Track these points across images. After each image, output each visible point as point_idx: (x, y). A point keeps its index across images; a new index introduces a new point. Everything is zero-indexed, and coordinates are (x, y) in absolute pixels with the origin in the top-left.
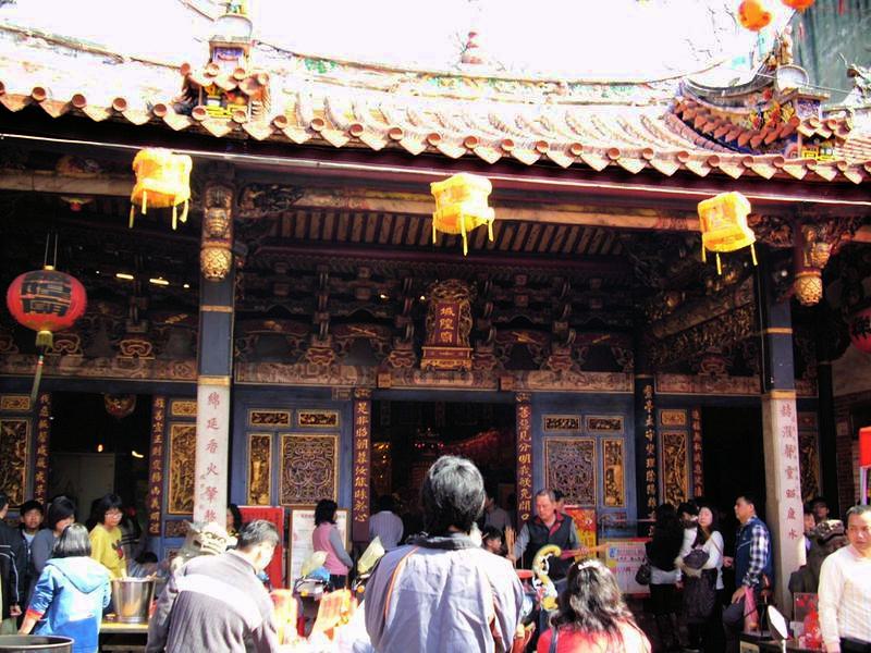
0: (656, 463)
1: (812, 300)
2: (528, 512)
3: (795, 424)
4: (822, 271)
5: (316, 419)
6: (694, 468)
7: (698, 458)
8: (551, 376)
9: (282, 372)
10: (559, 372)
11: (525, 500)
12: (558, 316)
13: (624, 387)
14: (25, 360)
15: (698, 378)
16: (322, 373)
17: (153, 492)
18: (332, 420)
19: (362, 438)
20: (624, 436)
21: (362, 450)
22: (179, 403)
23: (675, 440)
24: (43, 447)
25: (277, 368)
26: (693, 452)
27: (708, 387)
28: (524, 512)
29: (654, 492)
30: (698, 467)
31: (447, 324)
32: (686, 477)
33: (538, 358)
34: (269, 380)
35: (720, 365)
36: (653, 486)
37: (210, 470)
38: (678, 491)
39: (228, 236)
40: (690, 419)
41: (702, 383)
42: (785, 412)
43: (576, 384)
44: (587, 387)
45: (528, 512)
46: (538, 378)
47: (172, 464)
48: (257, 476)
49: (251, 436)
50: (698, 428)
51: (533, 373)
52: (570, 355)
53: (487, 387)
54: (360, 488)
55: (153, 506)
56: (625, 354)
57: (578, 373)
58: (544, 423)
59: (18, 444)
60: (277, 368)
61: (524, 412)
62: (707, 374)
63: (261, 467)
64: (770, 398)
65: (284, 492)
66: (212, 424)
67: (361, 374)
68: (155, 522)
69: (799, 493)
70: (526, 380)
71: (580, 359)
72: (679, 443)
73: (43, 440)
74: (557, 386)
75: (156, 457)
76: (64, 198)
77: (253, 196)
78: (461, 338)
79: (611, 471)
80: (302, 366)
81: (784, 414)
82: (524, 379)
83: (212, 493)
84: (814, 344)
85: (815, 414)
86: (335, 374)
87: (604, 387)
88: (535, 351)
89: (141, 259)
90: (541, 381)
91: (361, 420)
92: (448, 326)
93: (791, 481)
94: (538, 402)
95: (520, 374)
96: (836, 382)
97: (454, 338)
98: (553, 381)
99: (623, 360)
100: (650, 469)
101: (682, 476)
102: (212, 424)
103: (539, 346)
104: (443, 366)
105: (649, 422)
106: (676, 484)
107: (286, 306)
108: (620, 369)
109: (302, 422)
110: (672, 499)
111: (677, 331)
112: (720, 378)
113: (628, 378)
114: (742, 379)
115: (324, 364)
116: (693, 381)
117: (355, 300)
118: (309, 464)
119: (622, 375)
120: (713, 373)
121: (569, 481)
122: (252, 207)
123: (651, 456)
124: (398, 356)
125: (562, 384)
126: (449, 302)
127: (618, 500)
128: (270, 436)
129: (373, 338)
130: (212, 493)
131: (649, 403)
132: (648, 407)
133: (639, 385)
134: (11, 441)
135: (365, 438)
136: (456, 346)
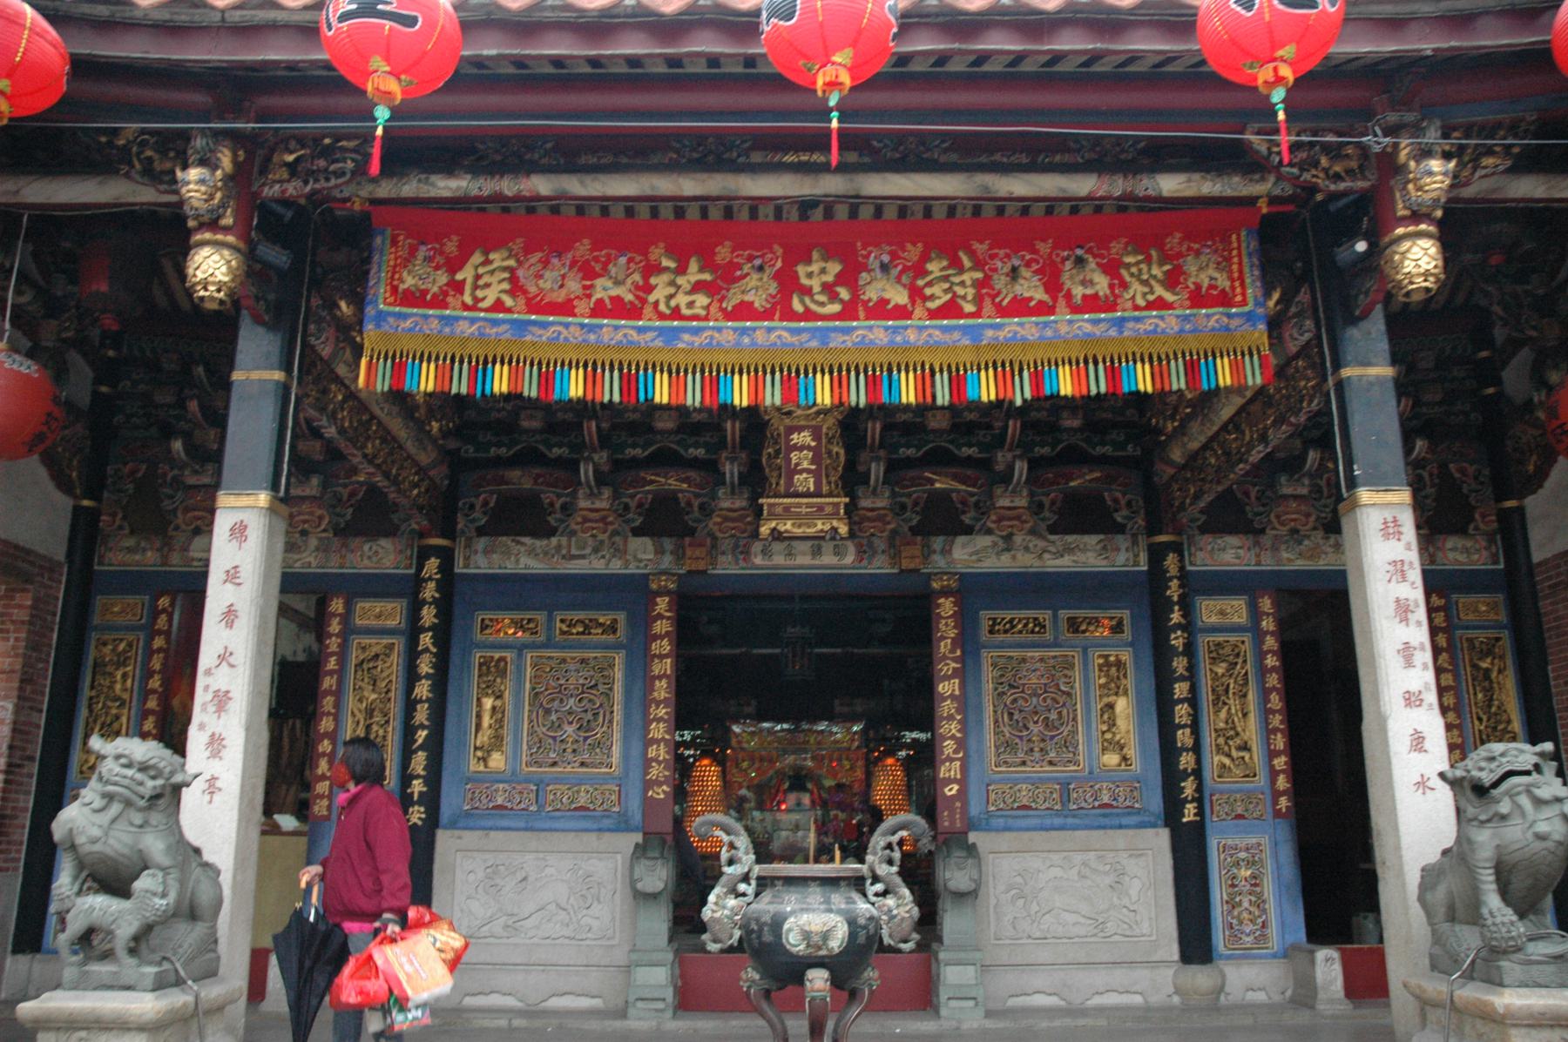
0: (1193, 689)
1: (1420, 282)
2: (955, 781)
4: (1440, 223)
5: (586, 627)
6: (1266, 700)
7: (1273, 680)
8: (995, 544)
9: (532, 552)
10: (1008, 538)
11: (952, 760)
12: (1000, 441)
13: (1122, 557)
14: (138, 544)
15: (1266, 540)
16: (596, 550)
17: (321, 749)
19: (662, 657)
20: (1131, 644)
21: (660, 678)
22: (367, 605)
23: (1227, 650)
24: (157, 677)
25: (523, 544)
26: (1263, 671)
27: (1285, 555)
28: (949, 781)
29: (1189, 742)
30: (1274, 697)
31: (802, 459)
32: (1252, 716)
33: (972, 514)
34: (510, 567)
35: (1308, 515)
36: (1188, 731)
37: (222, 658)
38: (1238, 741)
39: (228, 220)
40: (1255, 614)
41: (1275, 549)
42: (1390, 530)
43: (1040, 557)
44: (1058, 562)
45: (955, 781)
46: (970, 550)
47: (351, 702)
49: (477, 656)
50: (1272, 628)
51: (960, 540)
52: (1028, 508)
53: (880, 566)
54: (658, 742)
55: (320, 772)
56: (1129, 504)
57: (1045, 538)
58: (985, 625)
59: (119, 675)
60: (523, 544)
61: (947, 607)
62: (1283, 530)
63: (494, 708)
64: (1355, 505)
65: (530, 748)
66: (232, 576)
67: (660, 551)
68: (322, 797)
69: (1432, 697)
70: (950, 552)
71: (1047, 514)
72: (1238, 655)
73: (157, 667)
75: (328, 692)
77: (290, 158)
78: (829, 483)
79: (1111, 706)
80: (564, 540)
81: (1387, 536)
82: (946, 552)
84: (1487, 472)
85: (1500, 597)
86: (620, 552)
87: (1092, 561)
88: (964, 503)
90: (976, 553)
91: (661, 627)
92: (805, 465)
93: (1412, 672)
94: (977, 591)
95: (938, 542)
96: (1536, 535)
97: (818, 484)
98: (998, 554)
99: (1125, 512)
100: (1181, 701)
101: (1245, 715)
102: (232, 576)
103: (972, 495)
104: (798, 531)
105: (1176, 617)
106: (1234, 728)
107: (542, 448)
108: (1120, 529)
109: (563, 633)
110: (1229, 755)
111: (1203, 439)
112: (1308, 537)
113: (1135, 543)
115: (601, 537)
116: (1257, 543)
117: (651, 430)
118: (572, 701)
119: (1122, 541)
120: (1294, 531)
121: (1031, 726)
122: (286, 176)
123: (1182, 678)
124: (726, 519)
125: (1014, 557)
126: (802, 423)
127: (1125, 759)
129: (682, 491)
130: (221, 701)
131: (1174, 583)
132: (1174, 591)
133: (1156, 555)
134: (109, 669)
135: (666, 656)
136: (821, 496)
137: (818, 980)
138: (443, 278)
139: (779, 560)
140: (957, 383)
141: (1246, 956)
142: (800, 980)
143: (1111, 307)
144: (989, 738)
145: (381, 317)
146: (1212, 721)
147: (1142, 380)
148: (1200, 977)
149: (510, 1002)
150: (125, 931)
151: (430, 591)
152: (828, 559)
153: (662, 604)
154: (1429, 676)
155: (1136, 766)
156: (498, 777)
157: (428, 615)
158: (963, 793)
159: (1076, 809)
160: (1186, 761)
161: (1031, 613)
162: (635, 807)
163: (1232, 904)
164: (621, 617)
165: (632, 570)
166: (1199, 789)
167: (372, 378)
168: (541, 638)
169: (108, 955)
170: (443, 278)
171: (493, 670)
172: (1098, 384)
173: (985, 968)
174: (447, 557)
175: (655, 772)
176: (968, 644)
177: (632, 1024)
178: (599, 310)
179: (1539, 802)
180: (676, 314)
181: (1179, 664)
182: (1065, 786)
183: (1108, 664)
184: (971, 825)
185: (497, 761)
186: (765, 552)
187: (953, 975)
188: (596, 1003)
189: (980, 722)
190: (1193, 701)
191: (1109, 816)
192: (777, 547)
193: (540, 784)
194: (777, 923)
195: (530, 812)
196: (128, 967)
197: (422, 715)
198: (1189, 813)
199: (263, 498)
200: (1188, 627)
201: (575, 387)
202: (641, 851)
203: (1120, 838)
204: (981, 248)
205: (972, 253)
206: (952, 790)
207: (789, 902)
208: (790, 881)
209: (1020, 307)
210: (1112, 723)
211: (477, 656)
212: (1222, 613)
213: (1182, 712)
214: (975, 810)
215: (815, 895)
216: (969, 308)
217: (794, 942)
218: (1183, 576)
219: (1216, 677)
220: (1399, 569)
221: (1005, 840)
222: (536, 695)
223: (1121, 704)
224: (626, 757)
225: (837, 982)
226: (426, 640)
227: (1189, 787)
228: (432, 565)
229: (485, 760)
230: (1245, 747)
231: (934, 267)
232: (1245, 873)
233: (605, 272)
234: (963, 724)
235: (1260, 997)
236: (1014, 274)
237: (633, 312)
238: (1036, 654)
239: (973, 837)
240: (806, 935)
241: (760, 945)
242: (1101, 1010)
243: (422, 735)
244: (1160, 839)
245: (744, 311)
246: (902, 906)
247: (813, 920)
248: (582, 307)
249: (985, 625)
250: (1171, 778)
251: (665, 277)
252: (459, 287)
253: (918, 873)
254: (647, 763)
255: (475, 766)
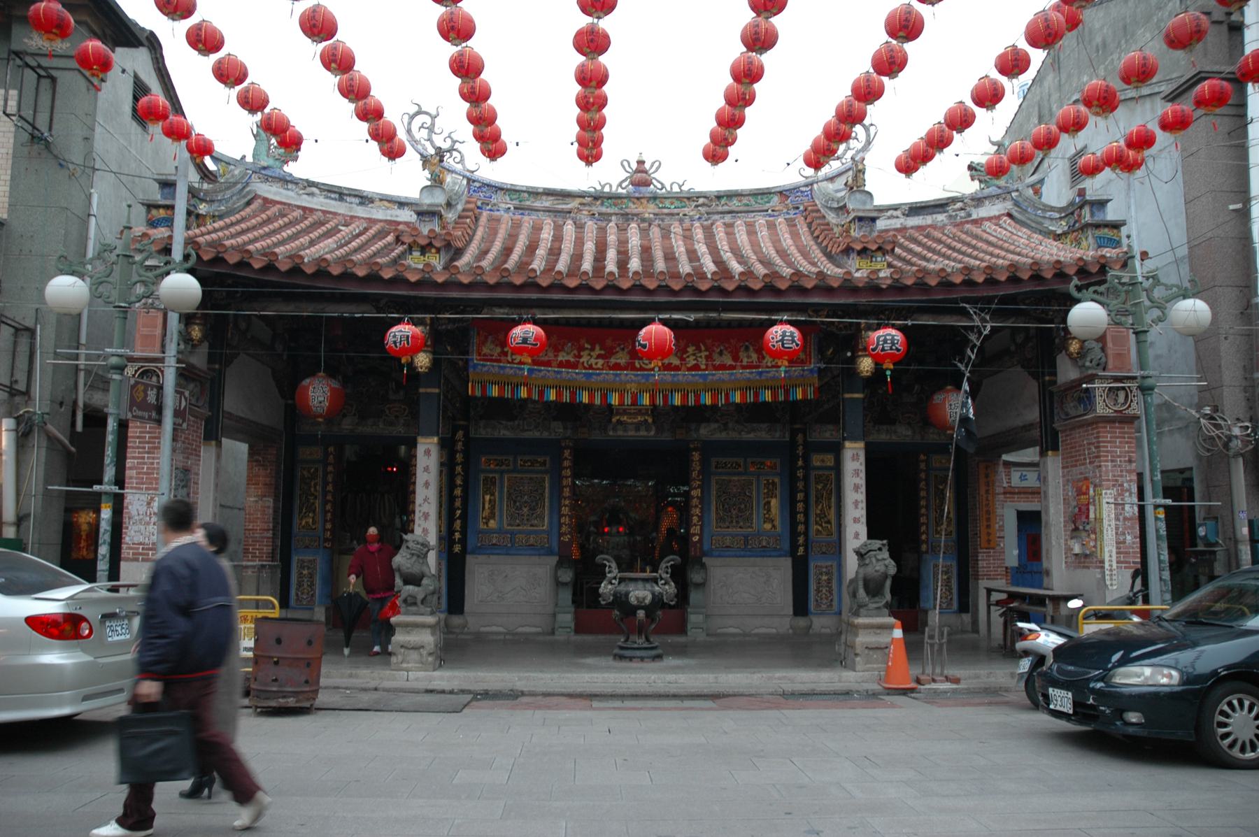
3: (863, 468)
10: (726, 424)
18: (544, 464)
34: (496, 435)
37: (425, 500)
48: (487, 506)
49: (482, 477)
51: (703, 425)
53: (666, 437)
58: (714, 464)
61: (696, 456)
66: (426, 469)
67: (565, 428)
69: (864, 520)
74: (723, 436)
76: (79, 428)
79: (769, 503)
83: (426, 516)
89: (634, 241)
94: (709, 449)
95: (693, 426)
102: (426, 469)
105: (800, 463)
114: (885, 427)
128: (497, 476)
130: (426, 516)
131: (801, 448)
132: (800, 451)
133: (794, 434)
137: (641, 614)
138: (498, 350)
139: (620, 433)
140: (697, 397)
141: (822, 613)
142: (634, 614)
143: (757, 367)
144: (713, 515)
145: (475, 366)
146: (814, 511)
147: (767, 396)
148: (802, 622)
149: (501, 629)
150: (420, 597)
151: (459, 446)
152: (643, 433)
153: (567, 453)
154: (864, 512)
155: (779, 529)
156: (492, 531)
157: (459, 457)
158: (701, 540)
159: (750, 548)
160: (801, 528)
161: (735, 459)
162: (555, 545)
163: (818, 591)
164: (548, 459)
165: (553, 437)
166: (806, 540)
167: (474, 390)
168: (511, 467)
169: (415, 604)
170: (498, 350)
171: (490, 484)
172: (750, 398)
173: (707, 616)
174: (466, 430)
175: (564, 529)
176: (705, 472)
177: (557, 637)
178: (561, 365)
179: (878, 560)
180: (591, 367)
181: (800, 485)
182: (746, 537)
183: (768, 483)
184: (705, 554)
185: (492, 524)
186: (614, 429)
187: (694, 618)
188: (539, 630)
189: (709, 509)
190: (806, 501)
191: (764, 552)
192: (619, 427)
193: (513, 533)
194: (627, 594)
195: (508, 546)
196: (422, 608)
197: (458, 503)
198: (801, 551)
199: (435, 439)
200: (807, 467)
201: (552, 396)
202: (560, 564)
203: (770, 561)
204: (709, 342)
205: (705, 345)
206: (696, 539)
207: (631, 587)
208: (631, 580)
209: (722, 367)
210: (769, 510)
211: (482, 477)
212: (823, 461)
213: (800, 506)
214: (706, 547)
215: (640, 585)
216: (703, 367)
217: (633, 600)
218: (806, 444)
219: (817, 490)
220: (857, 473)
221: (718, 561)
222: (509, 494)
223: (774, 502)
224: (550, 523)
225: (647, 616)
226: (459, 469)
227: (801, 540)
228: (460, 434)
229: (487, 523)
230: (829, 522)
231: (691, 349)
232: (825, 577)
233: (563, 350)
234: (702, 510)
235: (828, 631)
236: (721, 353)
237: (573, 366)
238: (736, 478)
239: (704, 559)
240: (637, 598)
241: (620, 601)
242: (756, 635)
243: (459, 512)
244: (786, 563)
245: (617, 367)
246: (671, 589)
247: (640, 593)
248: (554, 364)
249: (714, 464)
250: (794, 534)
251: (587, 352)
252: (506, 354)
253: (679, 576)
254: (560, 525)
255: (482, 526)
